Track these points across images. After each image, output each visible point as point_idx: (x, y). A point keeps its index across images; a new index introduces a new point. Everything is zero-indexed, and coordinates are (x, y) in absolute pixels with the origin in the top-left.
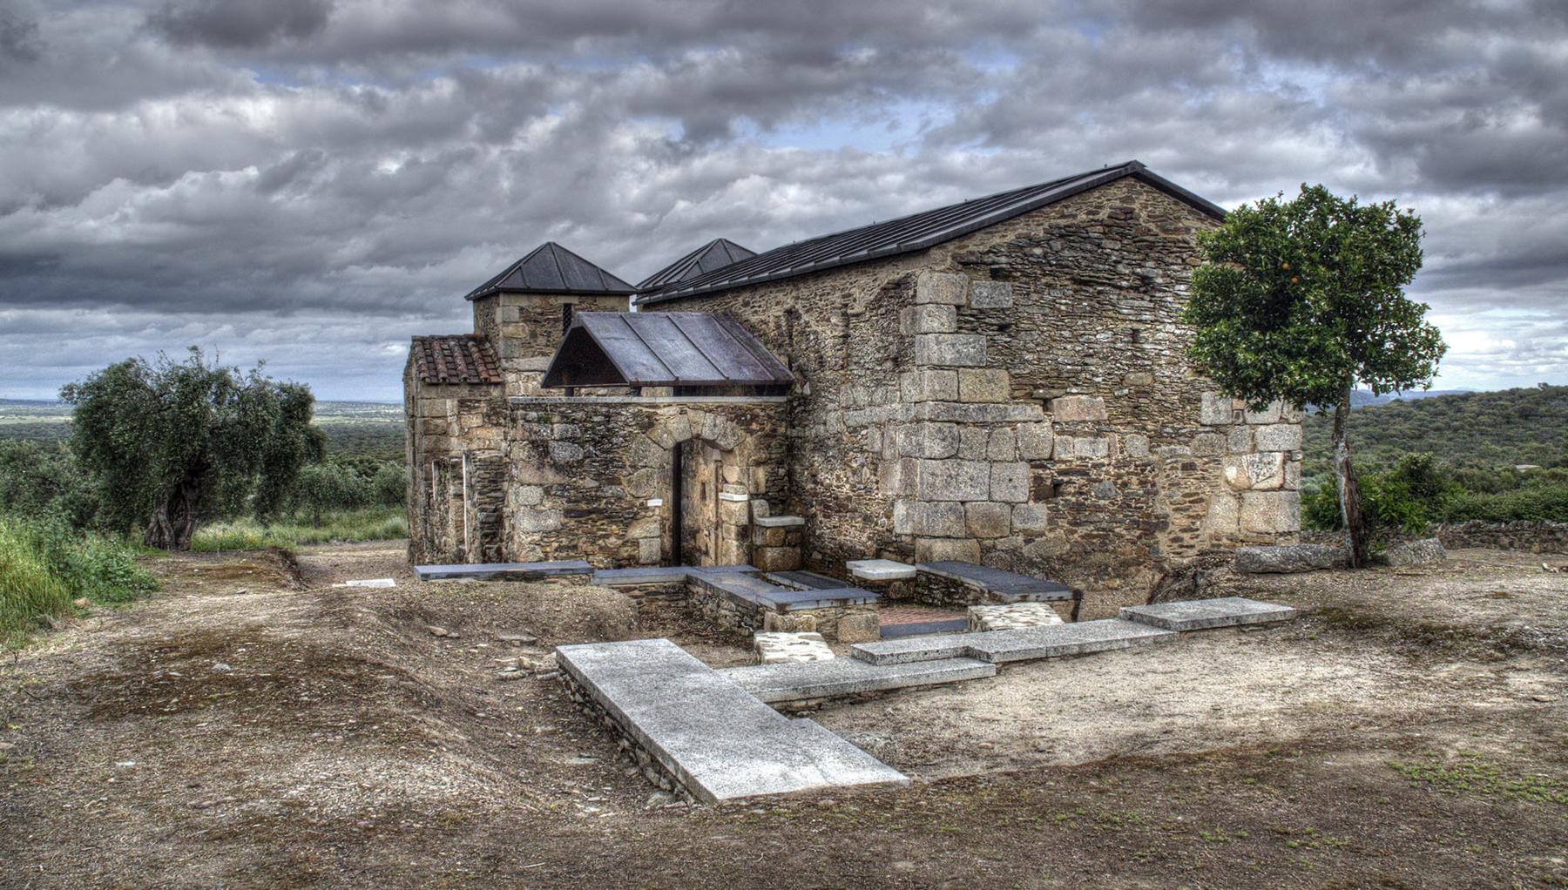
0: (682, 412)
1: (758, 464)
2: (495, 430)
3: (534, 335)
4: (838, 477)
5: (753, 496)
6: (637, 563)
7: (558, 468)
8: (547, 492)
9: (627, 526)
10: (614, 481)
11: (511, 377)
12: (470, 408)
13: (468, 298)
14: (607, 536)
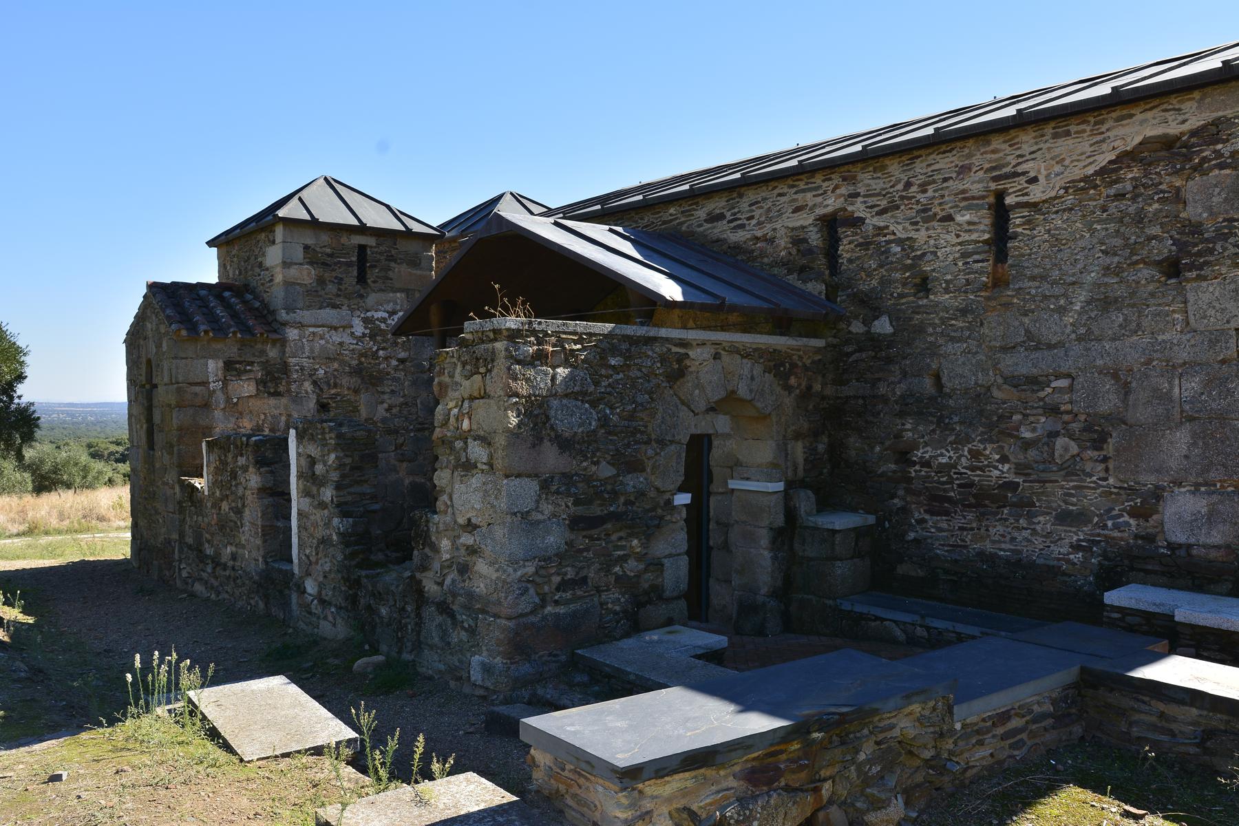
0: (716, 356)
1: (798, 436)
2: (272, 401)
3: (321, 281)
4: (975, 454)
5: (790, 485)
6: (660, 598)
7: (565, 444)
8: (545, 485)
9: (649, 537)
10: (635, 466)
11: (292, 334)
12: (239, 374)
13: (210, 243)
14: (624, 559)
